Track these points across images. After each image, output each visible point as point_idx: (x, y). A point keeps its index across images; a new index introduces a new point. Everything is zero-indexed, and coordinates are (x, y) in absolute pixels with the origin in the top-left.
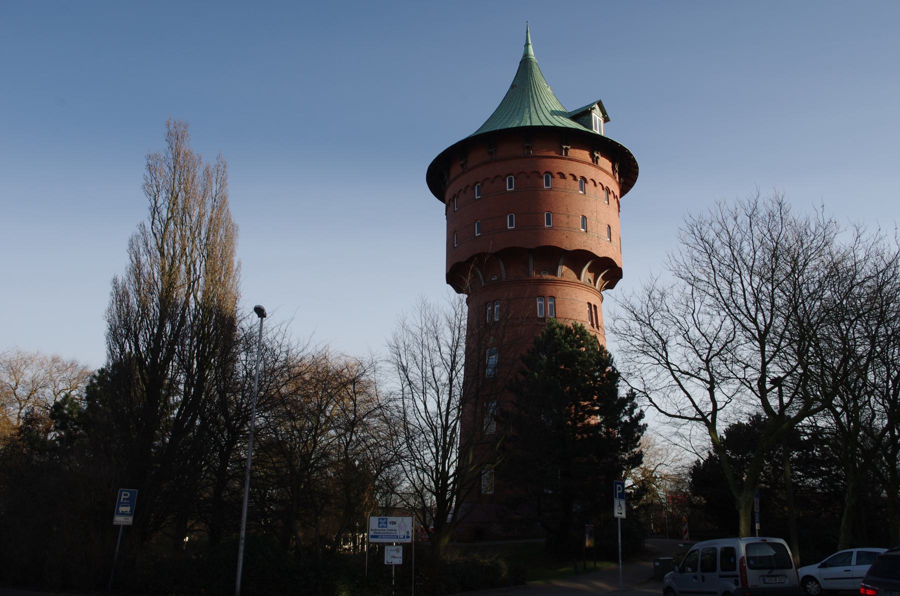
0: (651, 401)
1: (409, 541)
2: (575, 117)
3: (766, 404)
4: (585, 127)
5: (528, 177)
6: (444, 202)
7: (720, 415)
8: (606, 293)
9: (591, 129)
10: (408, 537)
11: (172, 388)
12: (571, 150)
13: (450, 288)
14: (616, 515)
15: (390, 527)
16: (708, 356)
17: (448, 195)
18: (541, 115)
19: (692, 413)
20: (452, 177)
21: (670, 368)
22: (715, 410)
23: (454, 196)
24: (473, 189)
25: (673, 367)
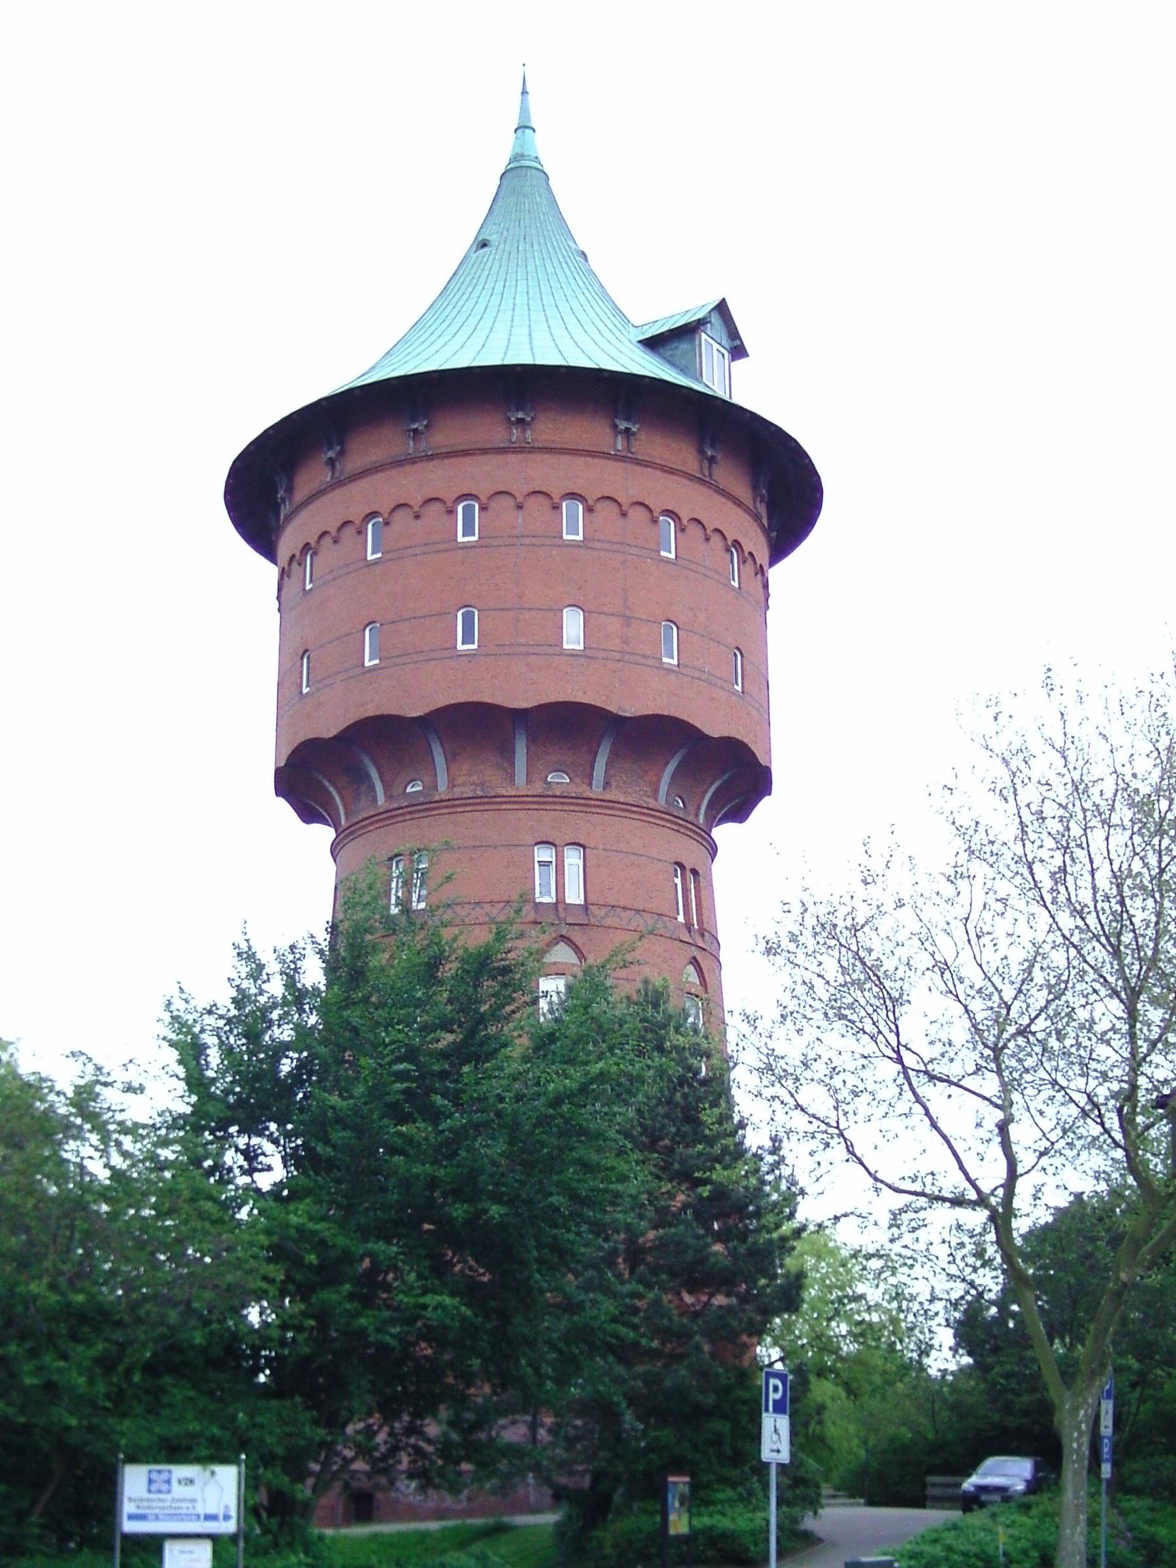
0: (850, 1150)
1: (230, 1527)
2: (653, 344)
3: (1134, 1166)
4: (684, 371)
5: (520, 507)
6: (276, 564)
7: (1023, 1187)
8: (723, 833)
9: (699, 378)
10: (227, 1517)
11: (625, 1261)
12: (643, 436)
13: (283, 805)
14: (766, 1455)
15: (178, 1491)
16: (999, 1037)
17: (288, 543)
18: (559, 332)
19: (951, 1182)
20: (300, 495)
21: (900, 1060)
22: (1010, 1185)
23: (306, 547)
24: (361, 532)
25: (909, 1060)
